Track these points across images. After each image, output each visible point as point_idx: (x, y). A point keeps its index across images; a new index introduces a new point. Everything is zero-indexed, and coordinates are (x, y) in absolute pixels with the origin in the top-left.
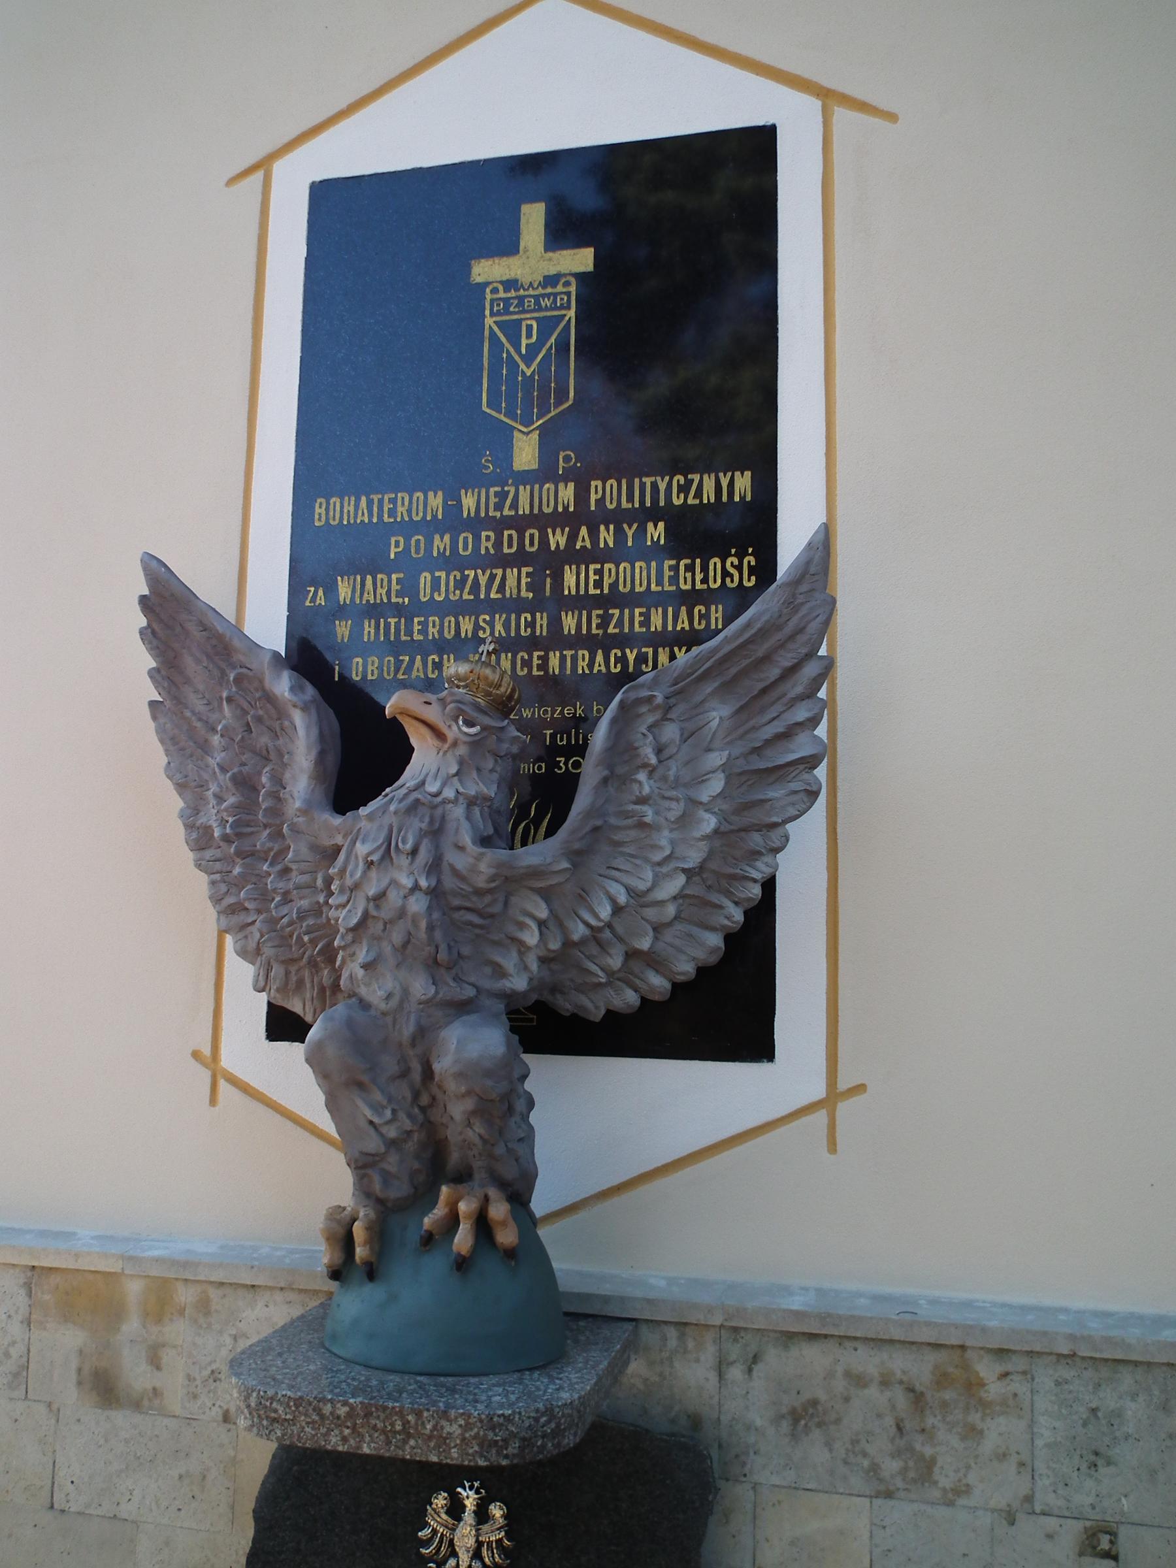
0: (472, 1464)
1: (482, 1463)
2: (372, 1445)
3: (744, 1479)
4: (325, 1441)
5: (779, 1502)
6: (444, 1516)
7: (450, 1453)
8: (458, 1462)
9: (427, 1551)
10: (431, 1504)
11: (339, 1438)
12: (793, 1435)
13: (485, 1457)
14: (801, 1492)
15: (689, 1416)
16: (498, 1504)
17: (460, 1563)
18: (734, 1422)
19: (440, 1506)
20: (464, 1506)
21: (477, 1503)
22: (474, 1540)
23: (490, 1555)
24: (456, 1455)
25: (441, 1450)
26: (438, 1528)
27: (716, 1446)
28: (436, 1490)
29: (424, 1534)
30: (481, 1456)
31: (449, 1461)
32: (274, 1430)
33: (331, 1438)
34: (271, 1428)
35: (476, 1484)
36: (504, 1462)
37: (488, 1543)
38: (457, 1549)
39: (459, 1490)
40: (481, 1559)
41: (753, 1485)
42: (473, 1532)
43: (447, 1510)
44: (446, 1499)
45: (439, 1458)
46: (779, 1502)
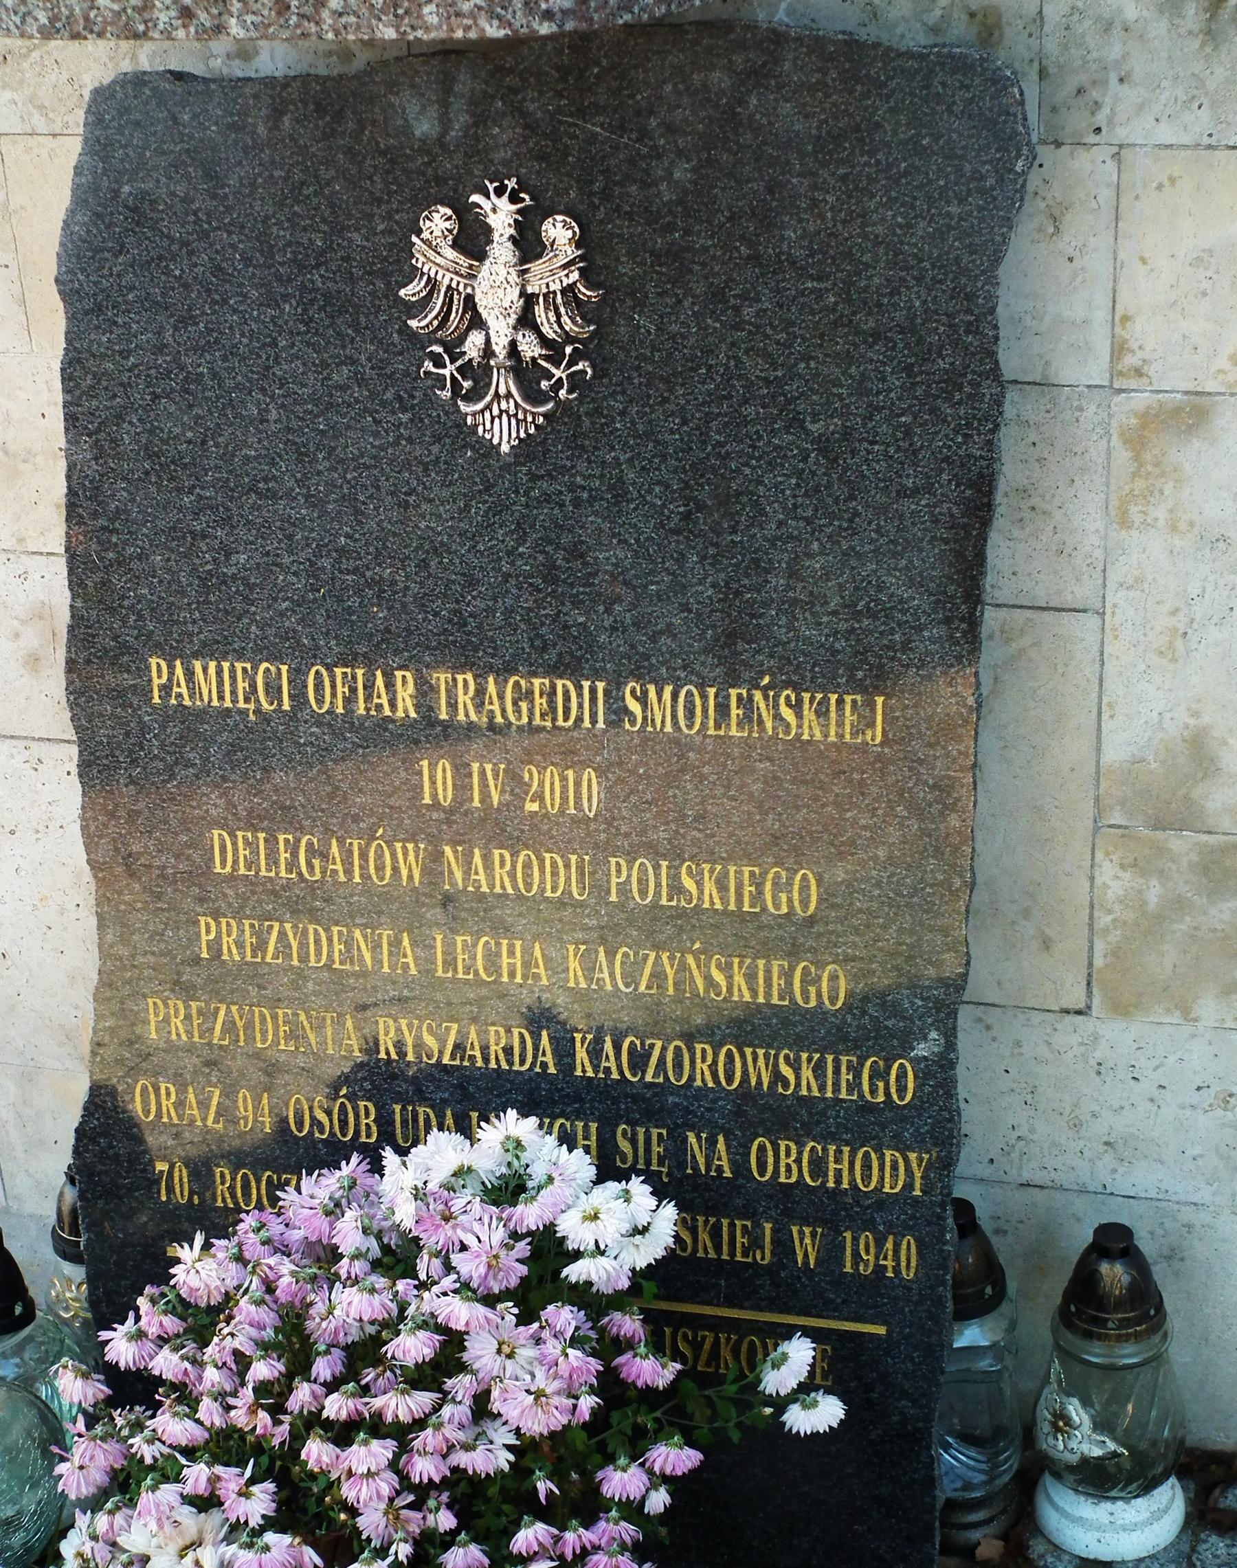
0: (472, 35)
1: (494, 31)
2: (249, 18)
3: (1092, 139)
4: (145, 22)
5: (1172, 180)
6: (450, 253)
7: (420, 16)
8: (443, 34)
9: (423, 323)
10: (419, 232)
11: (173, 13)
12: (1209, 32)
13: (499, 18)
14: (1221, 154)
15: (972, 15)
16: (559, 218)
17: (493, 340)
18: (1076, 17)
19: (437, 233)
20: (488, 230)
21: (516, 221)
22: (517, 291)
23: (553, 319)
24: (434, 20)
25: (400, 11)
26: (439, 277)
27: (1034, 75)
28: (426, 203)
29: (408, 292)
30: (492, 15)
31: (419, 34)
32: (29, 13)
33: (156, 14)
34: (23, 9)
35: (511, 184)
36: (545, 29)
37: (546, 296)
38: (484, 315)
39: (475, 198)
40: (536, 329)
41: (1116, 149)
42: (514, 277)
43: (454, 241)
44: (449, 219)
45: (397, 31)
46: (1172, 180)
